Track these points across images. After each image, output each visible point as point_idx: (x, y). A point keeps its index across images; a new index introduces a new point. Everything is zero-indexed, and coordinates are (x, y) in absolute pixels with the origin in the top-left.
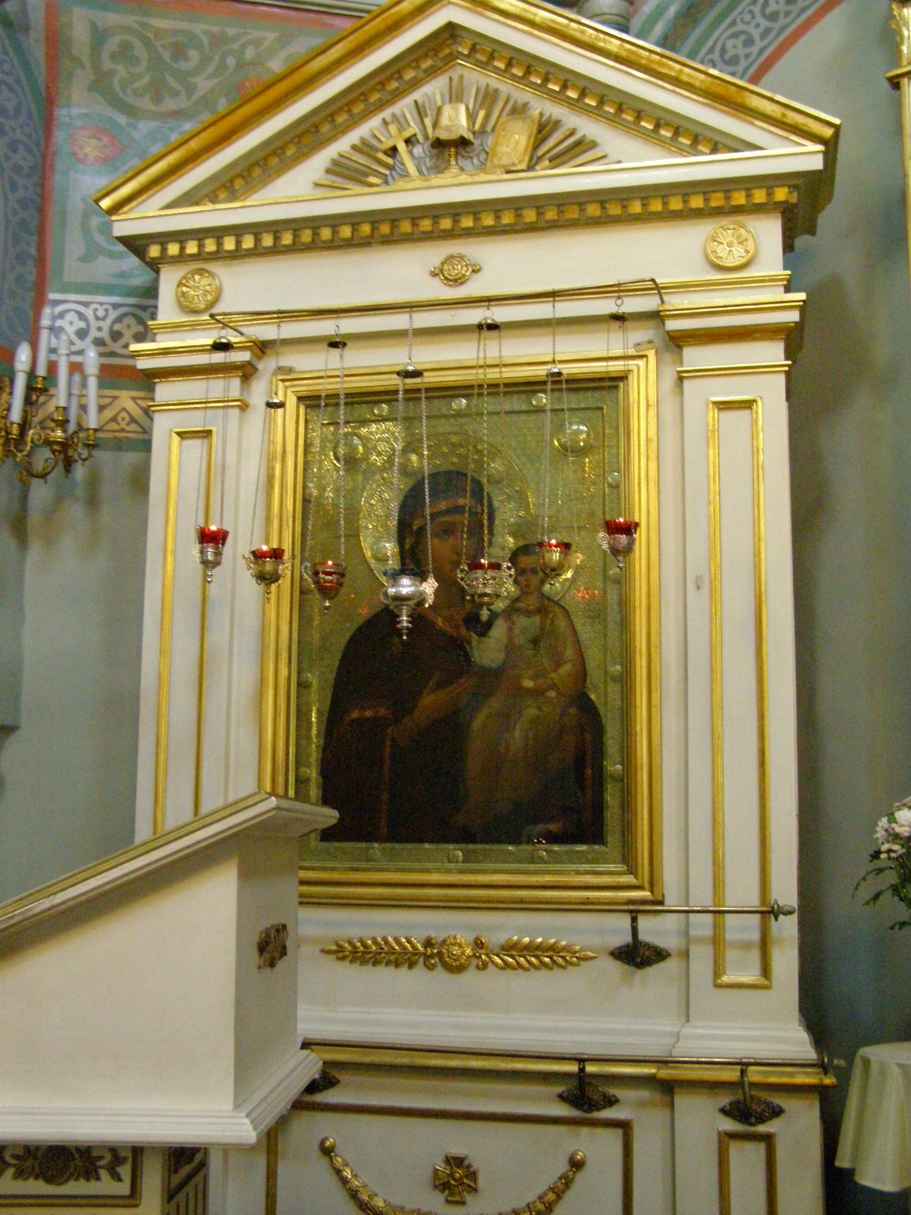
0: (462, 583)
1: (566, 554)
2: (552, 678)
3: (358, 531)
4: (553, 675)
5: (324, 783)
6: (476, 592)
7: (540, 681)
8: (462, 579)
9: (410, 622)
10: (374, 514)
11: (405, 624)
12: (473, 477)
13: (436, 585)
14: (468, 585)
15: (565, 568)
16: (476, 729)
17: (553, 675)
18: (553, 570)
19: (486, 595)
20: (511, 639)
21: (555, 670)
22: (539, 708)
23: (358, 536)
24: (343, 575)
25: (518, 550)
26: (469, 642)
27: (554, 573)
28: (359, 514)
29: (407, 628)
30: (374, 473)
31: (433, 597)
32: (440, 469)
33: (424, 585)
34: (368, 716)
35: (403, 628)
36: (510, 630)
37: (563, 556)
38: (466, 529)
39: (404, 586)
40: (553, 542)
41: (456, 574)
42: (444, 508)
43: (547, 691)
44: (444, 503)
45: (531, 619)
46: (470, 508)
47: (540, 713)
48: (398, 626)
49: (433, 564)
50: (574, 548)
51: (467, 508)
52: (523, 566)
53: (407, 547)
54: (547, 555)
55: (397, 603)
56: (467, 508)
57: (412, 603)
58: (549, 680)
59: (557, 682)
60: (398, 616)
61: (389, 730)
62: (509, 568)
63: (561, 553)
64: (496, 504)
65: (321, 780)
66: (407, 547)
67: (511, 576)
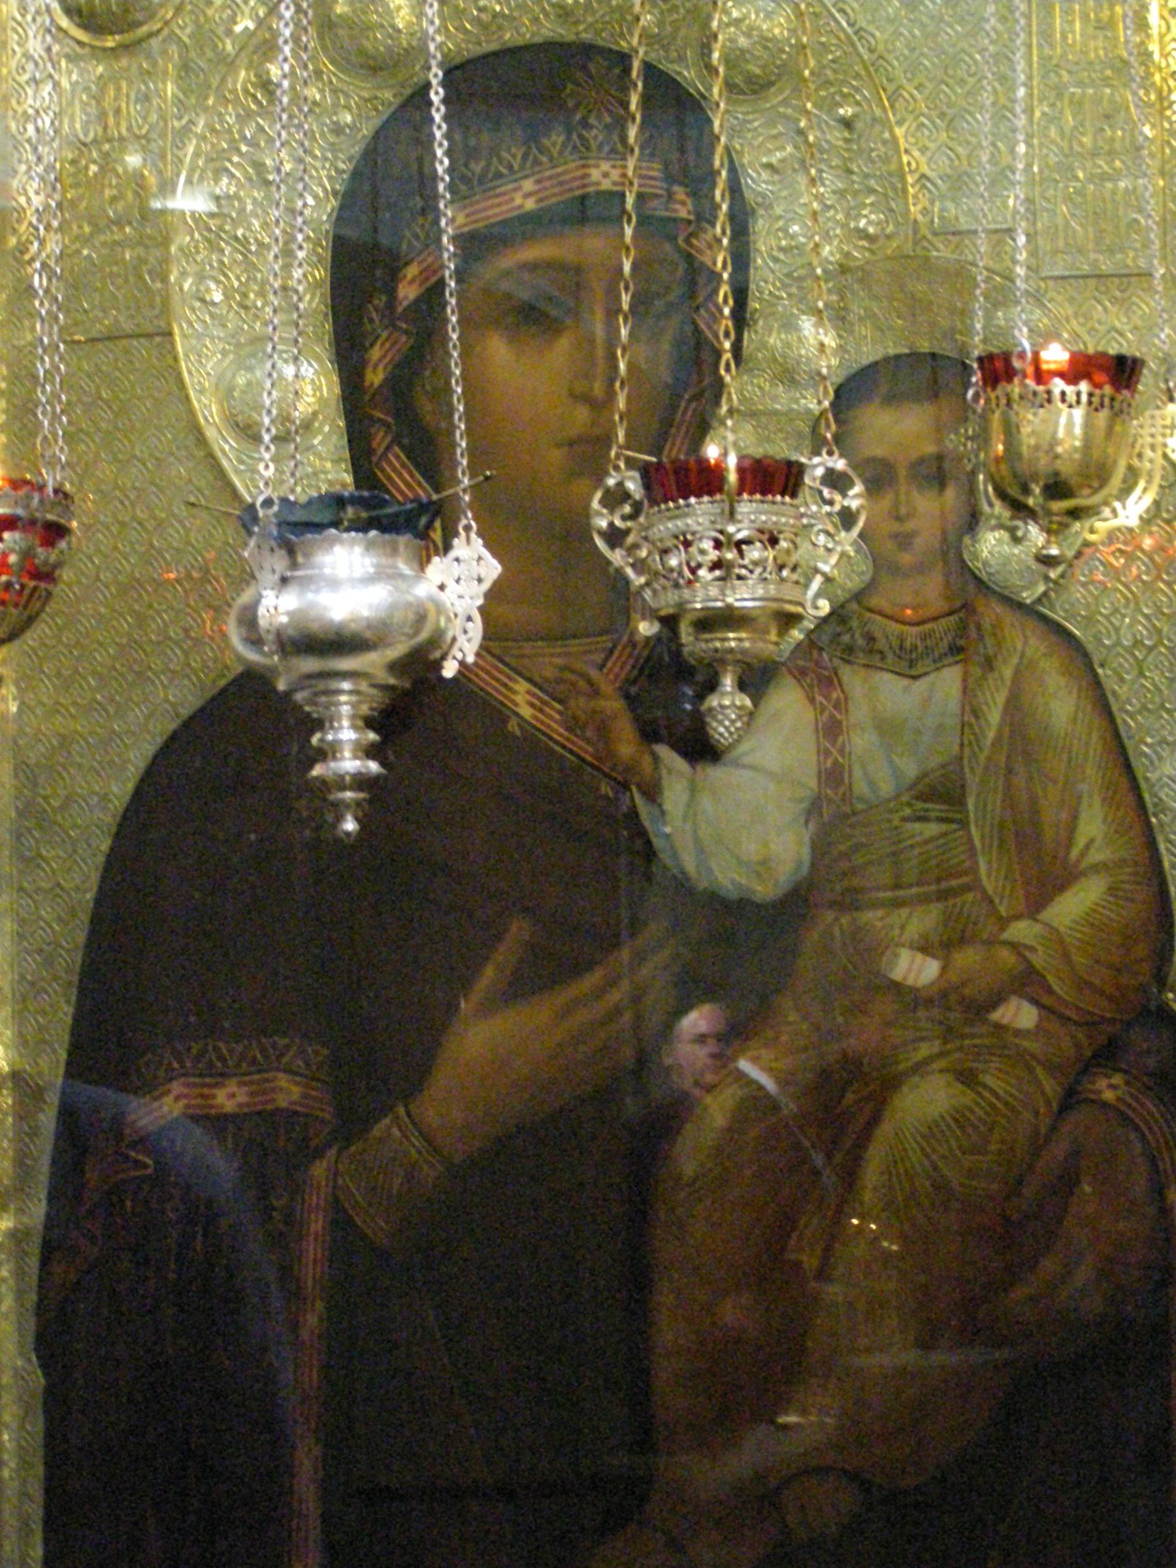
0: (617, 557)
1: (1119, 413)
2: (1014, 946)
3: (166, 309)
4: (1022, 931)
5: (50, 1392)
6: (681, 606)
7: (967, 958)
8: (615, 537)
9: (371, 751)
10: (874, 191)
11: (349, 764)
12: (649, 69)
13: (492, 569)
14: (640, 566)
15: (1116, 482)
16: (689, 1169)
17: (1022, 931)
18: (1057, 488)
19: (729, 619)
20: (833, 776)
21: (1036, 904)
22: (967, 1077)
23: (170, 334)
24: (54, 532)
25: (851, 379)
26: (652, 793)
27: (1058, 506)
28: (166, 242)
29: (361, 782)
30: (229, 64)
31: (476, 629)
32: (509, 37)
33: (438, 568)
34: (229, 1106)
35: (340, 783)
36: (831, 730)
37: (1103, 416)
38: (626, 300)
39: (334, 583)
40: (1055, 355)
41: (586, 514)
42: (530, 205)
43: (994, 1005)
44: (528, 185)
45: (921, 686)
46: (641, 198)
47: (967, 1098)
48: (317, 771)
49: (473, 470)
50: (1146, 383)
51: (630, 201)
52: (879, 452)
53: (375, 377)
54: (1031, 422)
55: (310, 664)
56: (630, 201)
57: (373, 662)
58: (1006, 957)
59: (1039, 960)
60: (319, 724)
61: (319, 1170)
62: (836, 481)
63: (1094, 407)
64: (757, 183)
65: (39, 1380)
66: (375, 377)
67: (847, 518)
